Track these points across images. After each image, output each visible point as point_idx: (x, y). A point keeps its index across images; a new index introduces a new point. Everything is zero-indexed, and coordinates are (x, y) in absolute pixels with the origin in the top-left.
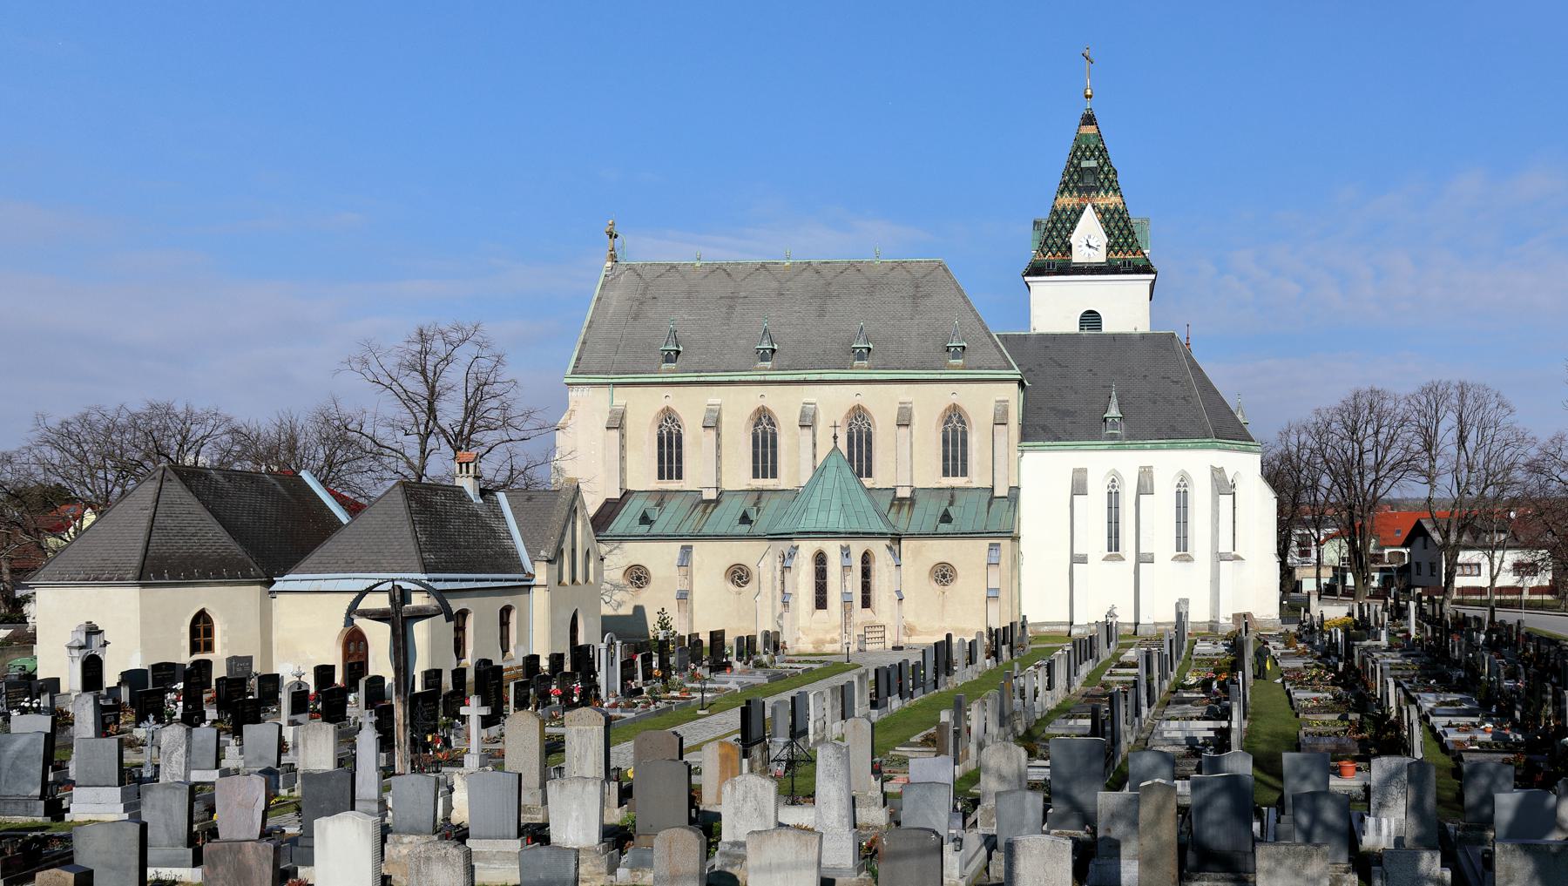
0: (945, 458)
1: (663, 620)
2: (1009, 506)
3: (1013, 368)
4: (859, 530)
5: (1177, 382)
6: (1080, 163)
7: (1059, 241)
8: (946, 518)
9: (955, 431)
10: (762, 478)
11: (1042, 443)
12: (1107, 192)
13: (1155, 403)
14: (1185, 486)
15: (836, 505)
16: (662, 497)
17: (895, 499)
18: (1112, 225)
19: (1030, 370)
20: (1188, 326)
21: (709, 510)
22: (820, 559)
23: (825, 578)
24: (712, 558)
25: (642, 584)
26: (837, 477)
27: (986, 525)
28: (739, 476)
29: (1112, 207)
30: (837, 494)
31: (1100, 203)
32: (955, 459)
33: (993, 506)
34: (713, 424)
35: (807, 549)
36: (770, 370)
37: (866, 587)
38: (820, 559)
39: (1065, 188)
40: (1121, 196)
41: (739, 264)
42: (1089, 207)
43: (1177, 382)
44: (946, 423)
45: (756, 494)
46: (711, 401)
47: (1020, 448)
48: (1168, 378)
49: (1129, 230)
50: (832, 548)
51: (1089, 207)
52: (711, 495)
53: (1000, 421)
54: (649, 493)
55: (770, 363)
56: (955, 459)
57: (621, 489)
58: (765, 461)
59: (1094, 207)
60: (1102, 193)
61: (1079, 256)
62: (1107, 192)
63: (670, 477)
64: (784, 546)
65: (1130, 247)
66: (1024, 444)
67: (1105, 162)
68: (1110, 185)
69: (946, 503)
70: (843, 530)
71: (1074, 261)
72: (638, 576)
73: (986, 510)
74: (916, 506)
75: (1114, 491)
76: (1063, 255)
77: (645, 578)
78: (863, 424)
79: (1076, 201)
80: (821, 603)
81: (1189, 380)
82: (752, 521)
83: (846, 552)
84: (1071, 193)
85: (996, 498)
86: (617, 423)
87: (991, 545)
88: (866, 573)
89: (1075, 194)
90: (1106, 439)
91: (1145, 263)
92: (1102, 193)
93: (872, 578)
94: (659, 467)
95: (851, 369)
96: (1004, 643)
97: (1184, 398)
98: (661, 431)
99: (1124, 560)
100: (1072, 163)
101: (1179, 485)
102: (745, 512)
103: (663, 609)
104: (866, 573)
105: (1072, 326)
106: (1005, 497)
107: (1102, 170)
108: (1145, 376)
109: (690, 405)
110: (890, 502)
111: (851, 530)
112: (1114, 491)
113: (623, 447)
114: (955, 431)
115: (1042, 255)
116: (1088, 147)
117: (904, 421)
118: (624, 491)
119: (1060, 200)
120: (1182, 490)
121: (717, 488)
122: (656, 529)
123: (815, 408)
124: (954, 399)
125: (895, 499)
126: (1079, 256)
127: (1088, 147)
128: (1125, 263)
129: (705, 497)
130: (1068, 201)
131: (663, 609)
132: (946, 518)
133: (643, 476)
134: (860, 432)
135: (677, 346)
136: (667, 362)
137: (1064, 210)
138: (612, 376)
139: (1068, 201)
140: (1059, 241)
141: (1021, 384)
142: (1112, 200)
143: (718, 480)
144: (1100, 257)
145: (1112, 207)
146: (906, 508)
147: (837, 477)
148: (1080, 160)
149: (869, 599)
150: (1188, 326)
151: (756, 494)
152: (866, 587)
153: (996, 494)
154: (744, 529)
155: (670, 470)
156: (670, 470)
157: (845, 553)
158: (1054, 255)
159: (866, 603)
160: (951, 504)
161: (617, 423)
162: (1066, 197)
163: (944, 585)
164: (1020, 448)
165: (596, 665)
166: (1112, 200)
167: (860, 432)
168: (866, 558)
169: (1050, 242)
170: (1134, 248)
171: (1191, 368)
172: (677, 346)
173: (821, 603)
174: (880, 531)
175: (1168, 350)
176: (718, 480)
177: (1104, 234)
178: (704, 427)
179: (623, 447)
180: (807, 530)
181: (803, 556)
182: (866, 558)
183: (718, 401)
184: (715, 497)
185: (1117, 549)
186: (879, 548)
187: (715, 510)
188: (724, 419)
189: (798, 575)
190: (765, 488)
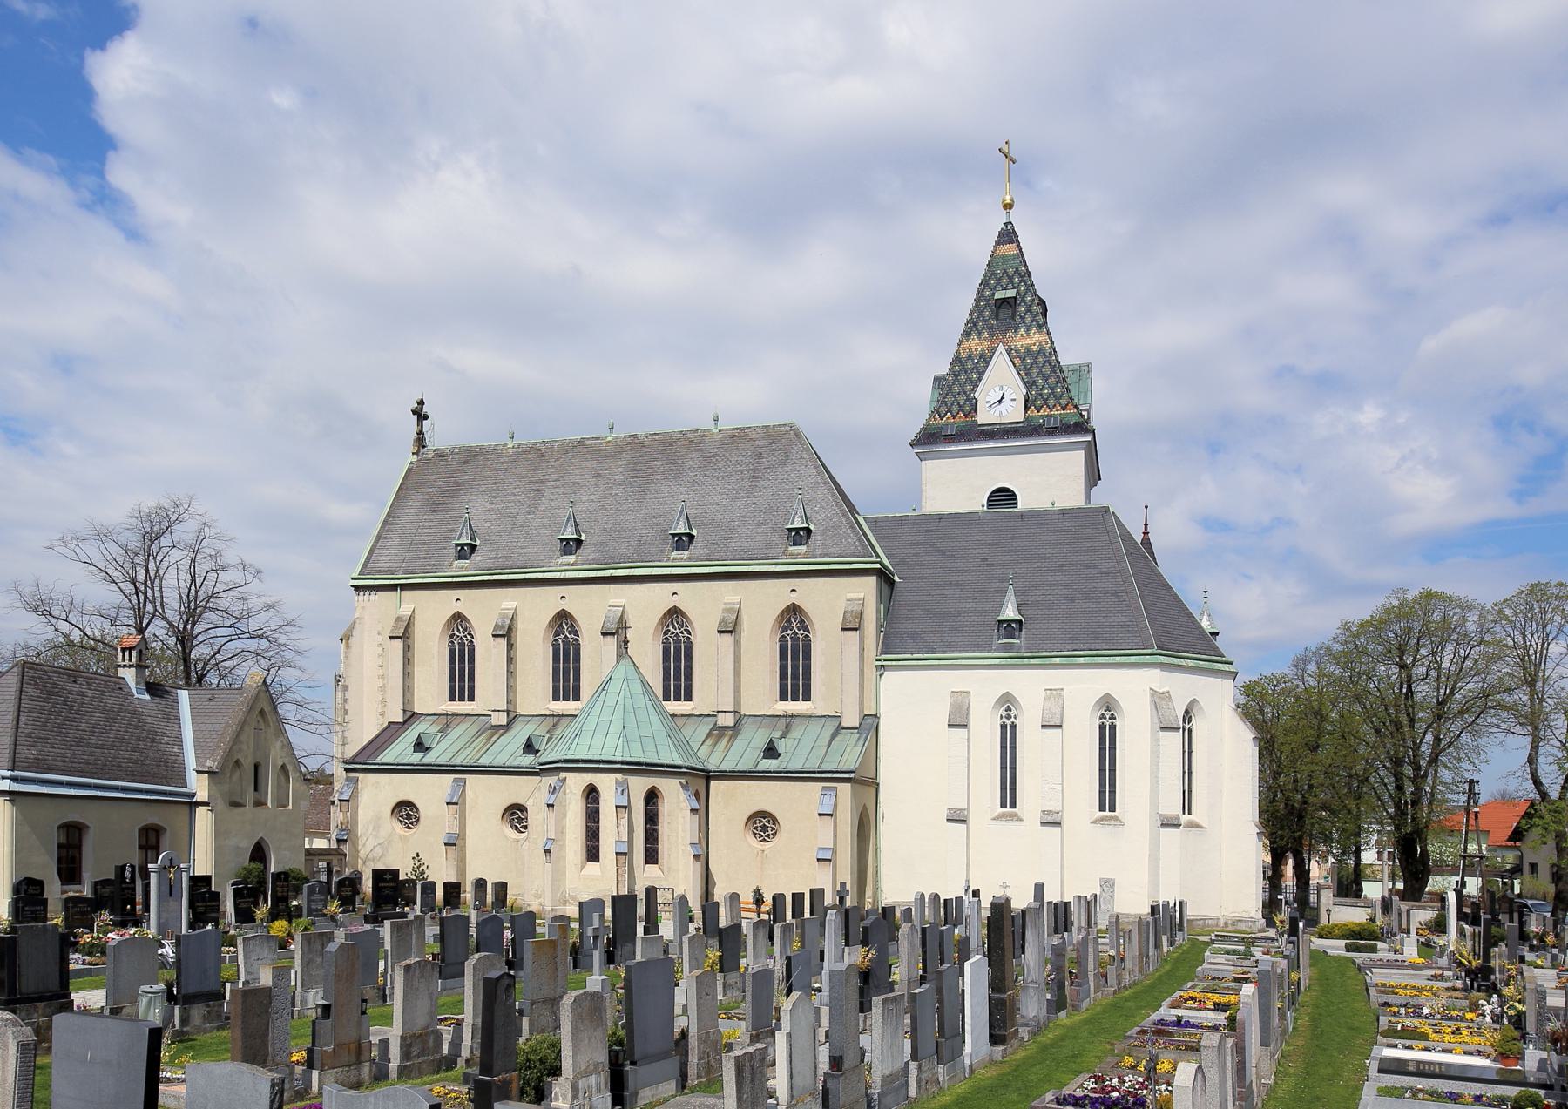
0: (783, 676)
1: (418, 868)
2: (859, 739)
3: (872, 556)
4: (642, 760)
5: (1107, 573)
6: (993, 295)
7: (962, 398)
8: (771, 752)
9: (795, 639)
10: (574, 700)
11: (909, 656)
12: (1028, 329)
13: (1073, 601)
14: (1112, 717)
15: (616, 727)
16: (448, 720)
17: (715, 727)
18: (1035, 371)
19: (903, 561)
20: (1146, 507)
21: (494, 738)
22: (592, 793)
23: (598, 822)
24: (488, 795)
25: (411, 823)
26: (623, 691)
27: (820, 765)
28: (762, 696)
29: (1035, 348)
30: (619, 714)
31: (1019, 344)
32: (795, 677)
33: (837, 739)
34: (507, 633)
35: (576, 782)
36: (572, 565)
37: (652, 837)
38: (592, 793)
39: (971, 328)
40: (1049, 333)
41: (556, 442)
42: (1001, 348)
43: (1107, 573)
44: (784, 629)
45: (443, 720)
46: (505, 605)
47: (879, 663)
48: (1095, 567)
49: (1058, 377)
50: (606, 784)
51: (1001, 348)
52: (728, 720)
53: (852, 624)
54: (436, 717)
55: (573, 557)
56: (795, 677)
57: (404, 711)
58: (566, 680)
59: (1009, 352)
60: (1022, 331)
61: (986, 416)
62: (1028, 329)
63: (462, 699)
64: (552, 780)
65: (1057, 399)
66: (884, 656)
67: (1027, 290)
68: (1033, 320)
69: (777, 734)
70: (620, 759)
71: (979, 423)
72: (406, 811)
73: (827, 742)
74: (739, 737)
75: (1008, 723)
76: (966, 416)
77: (773, 829)
78: (682, 633)
79: (986, 344)
80: (593, 855)
81: (1125, 570)
82: (538, 751)
83: (624, 789)
84: (979, 335)
85: (843, 728)
86: (404, 634)
87: (823, 787)
88: (652, 818)
89: (986, 335)
90: (998, 650)
91: (1076, 419)
92: (1022, 331)
93: (660, 824)
94: (450, 687)
95: (667, 561)
96: (1349, 948)
97: (1115, 594)
98: (452, 642)
99: (1021, 820)
100: (983, 295)
101: (1103, 717)
102: (529, 739)
103: (418, 855)
104: (652, 818)
105: (976, 502)
106: (855, 728)
107: (1023, 300)
108: (1062, 566)
109: (484, 609)
110: (708, 731)
111: (629, 759)
112: (1008, 723)
113: (511, 660)
114: (795, 639)
115: (938, 417)
116: (1005, 272)
117: (730, 628)
118: (409, 714)
119: (966, 345)
120: (1108, 722)
121: (508, 712)
122: (430, 758)
123: (623, 612)
124: (794, 598)
125: (715, 727)
126: (986, 416)
127: (1005, 272)
128: (1049, 421)
129: (494, 722)
130: (976, 345)
131: (418, 855)
132: (771, 751)
133: (432, 694)
134: (677, 642)
135: (690, 529)
136: (460, 558)
137: (970, 356)
138: (400, 576)
139: (976, 345)
140: (962, 398)
141: (884, 576)
142: (1036, 339)
143: (737, 701)
144: (1013, 412)
145: (1035, 348)
146: (725, 740)
147: (623, 691)
148: (994, 290)
149: (657, 853)
150: (1146, 507)
151: (443, 720)
152: (652, 837)
153: (844, 724)
154: (528, 760)
155: (678, 688)
156: (678, 688)
157: (620, 789)
158: (954, 417)
159: (652, 857)
160: (783, 736)
161: (404, 634)
162: (973, 340)
163: (764, 841)
164: (879, 663)
165: (139, 898)
166: (1036, 339)
167: (462, 645)
168: (652, 796)
169: (949, 400)
170: (1063, 402)
171: (1129, 554)
172: (690, 529)
173: (593, 855)
174: (672, 762)
175: (1098, 529)
176: (737, 701)
177: (1021, 384)
178: (494, 636)
179: (511, 660)
180: (577, 757)
181: (571, 791)
182: (652, 796)
183: (621, 602)
184: (732, 724)
185: (1013, 805)
186: (671, 789)
187: (502, 737)
188: (520, 626)
189: (565, 816)
190: (795, 713)
